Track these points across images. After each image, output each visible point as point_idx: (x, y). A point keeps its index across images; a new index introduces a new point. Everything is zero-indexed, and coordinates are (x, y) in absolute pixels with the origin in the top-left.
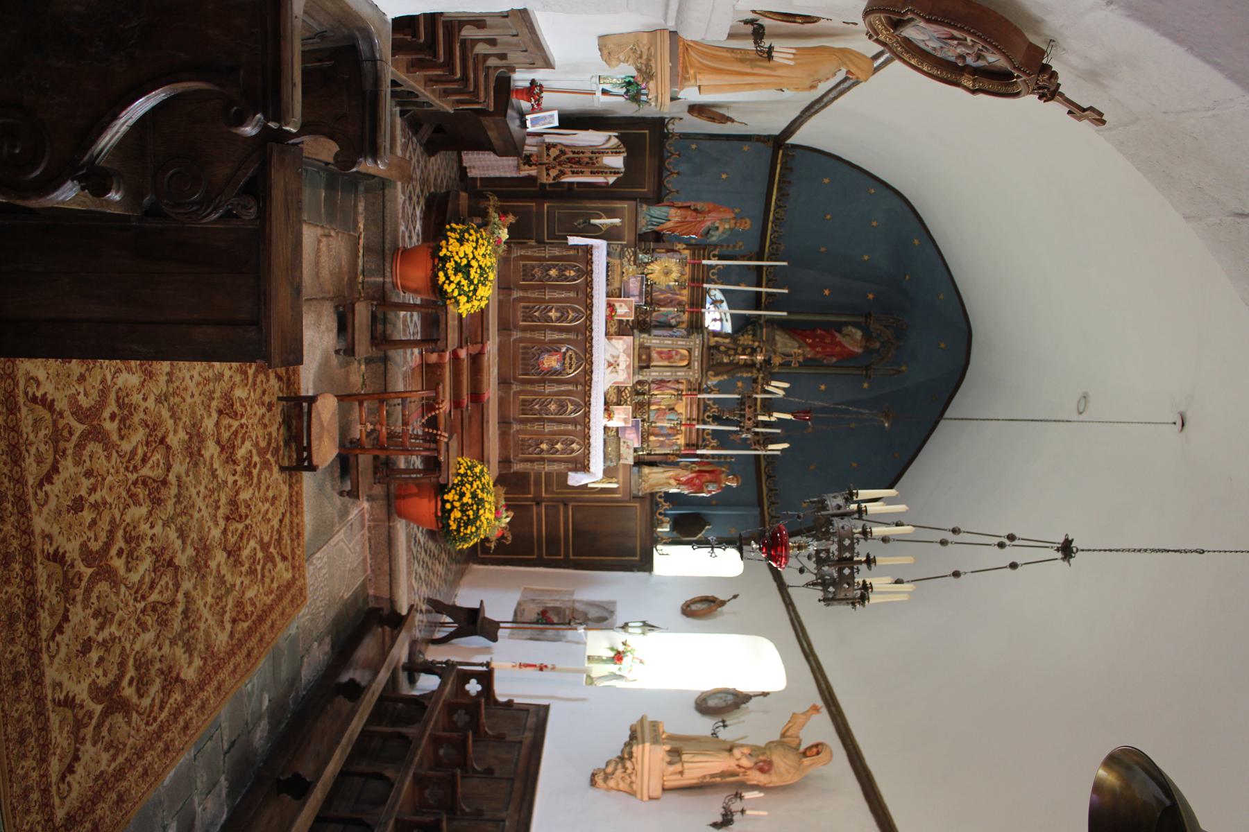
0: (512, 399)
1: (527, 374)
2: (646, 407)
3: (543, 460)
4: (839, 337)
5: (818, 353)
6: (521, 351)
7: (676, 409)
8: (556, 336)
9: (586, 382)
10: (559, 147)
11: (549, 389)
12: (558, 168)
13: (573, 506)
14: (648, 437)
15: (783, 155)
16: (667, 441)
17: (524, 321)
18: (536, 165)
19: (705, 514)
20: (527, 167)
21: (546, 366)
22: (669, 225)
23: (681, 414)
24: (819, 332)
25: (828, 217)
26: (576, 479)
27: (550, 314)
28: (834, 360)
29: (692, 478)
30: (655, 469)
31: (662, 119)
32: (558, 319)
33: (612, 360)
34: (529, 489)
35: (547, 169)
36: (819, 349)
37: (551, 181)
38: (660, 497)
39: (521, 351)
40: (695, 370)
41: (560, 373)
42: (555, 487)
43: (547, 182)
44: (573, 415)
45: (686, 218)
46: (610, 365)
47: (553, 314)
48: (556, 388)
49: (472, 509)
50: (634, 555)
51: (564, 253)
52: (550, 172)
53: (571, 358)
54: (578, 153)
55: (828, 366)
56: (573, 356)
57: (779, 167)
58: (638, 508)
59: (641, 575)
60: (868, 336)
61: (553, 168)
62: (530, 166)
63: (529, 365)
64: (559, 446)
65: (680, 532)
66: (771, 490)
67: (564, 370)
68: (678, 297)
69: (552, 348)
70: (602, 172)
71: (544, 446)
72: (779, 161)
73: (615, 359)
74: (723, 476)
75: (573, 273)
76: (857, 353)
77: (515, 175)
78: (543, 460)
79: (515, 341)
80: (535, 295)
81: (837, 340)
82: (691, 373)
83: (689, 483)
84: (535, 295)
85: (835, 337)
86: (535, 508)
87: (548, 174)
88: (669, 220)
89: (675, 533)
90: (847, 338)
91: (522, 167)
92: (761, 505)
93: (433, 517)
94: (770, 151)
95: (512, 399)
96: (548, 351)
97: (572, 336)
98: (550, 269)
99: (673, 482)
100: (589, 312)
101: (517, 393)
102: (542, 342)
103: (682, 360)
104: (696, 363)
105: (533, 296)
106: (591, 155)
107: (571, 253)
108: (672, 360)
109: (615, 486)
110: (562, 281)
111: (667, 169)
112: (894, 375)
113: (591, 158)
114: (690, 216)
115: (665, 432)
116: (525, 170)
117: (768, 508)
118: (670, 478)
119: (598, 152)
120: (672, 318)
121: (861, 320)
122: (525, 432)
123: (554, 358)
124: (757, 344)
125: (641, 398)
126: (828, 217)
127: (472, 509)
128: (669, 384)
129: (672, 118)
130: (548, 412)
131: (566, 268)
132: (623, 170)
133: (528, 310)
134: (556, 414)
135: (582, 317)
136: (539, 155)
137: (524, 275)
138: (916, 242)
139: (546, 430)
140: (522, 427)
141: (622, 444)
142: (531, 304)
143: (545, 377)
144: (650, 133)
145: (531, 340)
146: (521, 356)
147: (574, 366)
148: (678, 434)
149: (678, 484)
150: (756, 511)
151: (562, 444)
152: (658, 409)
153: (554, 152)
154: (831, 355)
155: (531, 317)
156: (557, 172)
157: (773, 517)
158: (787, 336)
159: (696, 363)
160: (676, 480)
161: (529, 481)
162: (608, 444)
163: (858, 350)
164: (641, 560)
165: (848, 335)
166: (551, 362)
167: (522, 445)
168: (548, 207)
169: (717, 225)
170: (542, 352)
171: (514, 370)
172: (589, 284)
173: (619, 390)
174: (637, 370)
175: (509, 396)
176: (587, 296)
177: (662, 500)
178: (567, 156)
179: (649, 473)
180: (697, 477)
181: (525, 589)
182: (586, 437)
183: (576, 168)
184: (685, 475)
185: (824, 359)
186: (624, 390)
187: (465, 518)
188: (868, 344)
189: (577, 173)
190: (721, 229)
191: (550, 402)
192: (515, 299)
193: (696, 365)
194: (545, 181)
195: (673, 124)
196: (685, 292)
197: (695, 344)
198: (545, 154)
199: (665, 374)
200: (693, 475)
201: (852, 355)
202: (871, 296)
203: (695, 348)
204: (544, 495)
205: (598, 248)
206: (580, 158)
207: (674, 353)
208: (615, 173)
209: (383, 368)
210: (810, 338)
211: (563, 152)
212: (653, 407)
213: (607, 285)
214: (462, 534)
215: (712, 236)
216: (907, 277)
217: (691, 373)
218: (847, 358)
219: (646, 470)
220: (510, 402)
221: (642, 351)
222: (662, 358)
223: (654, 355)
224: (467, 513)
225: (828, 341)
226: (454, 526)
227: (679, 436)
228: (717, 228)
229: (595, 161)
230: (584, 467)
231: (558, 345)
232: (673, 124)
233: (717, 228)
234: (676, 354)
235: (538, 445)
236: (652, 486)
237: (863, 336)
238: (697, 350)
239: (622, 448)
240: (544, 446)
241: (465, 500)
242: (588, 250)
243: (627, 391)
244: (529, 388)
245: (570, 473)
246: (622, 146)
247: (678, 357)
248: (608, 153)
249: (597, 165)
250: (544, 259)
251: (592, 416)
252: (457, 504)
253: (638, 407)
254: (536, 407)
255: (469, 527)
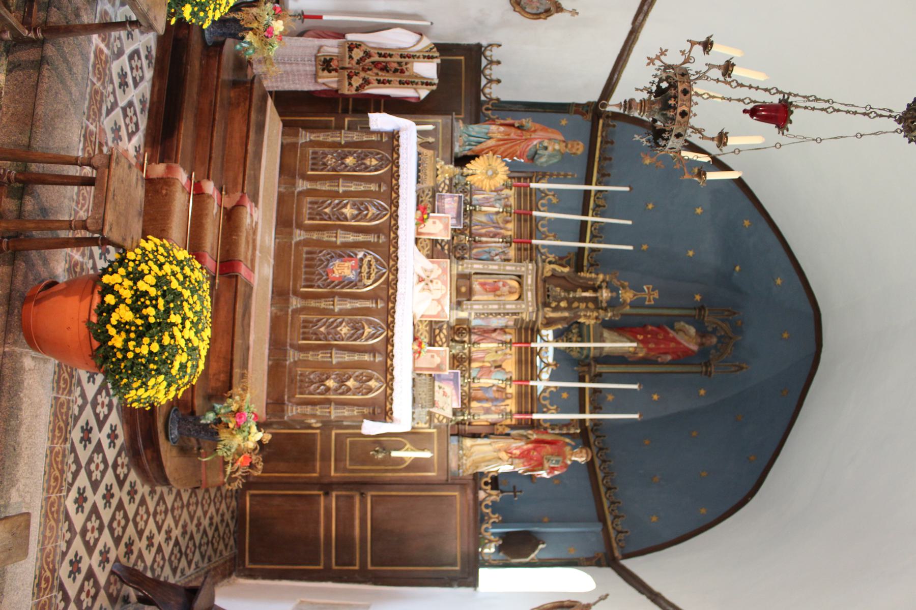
0: (290, 319)
1: (311, 287)
2: (466, 364)
3: (328, 402)
4: (672, 334)
5: (650, 350)
6: (304, 256)
7: (504, 366)
8: (351, 238)
9: (389, 297)
10: (363, 48)
11: (339, 305)
12: (362, 74)
13: (372, 496)
14: (469, 402)
15: (603, 124)
16: (493, 408)
17: (310, 219)
18: (336, 70)
19: (537, 533)
20: (326, 73)
21: (337, 275)
22: (491, 143)
23: (510, 372)
24: (650, 328)
25: (650, 206)
26: (371, 428)
27: (344, 210)
28: (669, 358)
29: (529, 451)
30: (479, 441)
31: (479, 46)
32: (354, 218)
33: (423, 275)
34: (314, 466)
35: (350, 77)
36: (652, 346)
37: (354, 92)
38: (487, 506)
39: (304, 256)
40: (528, 302)
41: (356, 285)
42: (348, 462)
43: (349, 93)
44: (371, 342)
45: (509, 135)
46: (421, 280)
47: (348, 211)
48: (349, 305)
49: (155, 307)
50: (454, 564)
51: (365, 139)
52: (353, 82)
53: (370, 266)
54: (385, 56)
55: (662, 364)
56: (373, 262)
57: (599, 140)
58: (458, 497)
59: (463, 592)
60: (702, 333)
61: (356, 74)
62: (330, 71)
63: (313, 273)
64: (351, 383)
65: (506, 553)
66: (613, 503)
67: (361, 281)
68: (502, 231)
69: (345, 252)
70: (412, 83)
71: (331, 383)
72: (599, 133)
73: (428, 273)
74: (568, 449)
75: (374, 162)
76: (693, 351)
77: (312, 87)
78: (328, 402)
79: (298, 244)
80: (326, 187)
81: (671, 335)
82: (523, 306)
83: (525, 455)
84: (326, 187)
85: (668, 333)
86: (322, 499)
87: (350, 84)
88: (490, 138)
89: (501, 554)
90: (681, 333)
91: (320, 73)
92: (602, 519)
93: (83, 327)
94: (588, 125)
95: (290, 319)
96: (340, 256)
97: (371, 238)
98: (346, 156)
99: (504, 455)
100: (394, 209)
101: (296, 311)
102: (333, 245)
103: (511, 293)
104: (529, 294)
105: (324, 188)
106: (400, 60)
107: (374, 138)
108: (498, 293)
109: (426, 454)
110: (360, 171)
111: (483, 113)
112: (736, 371)
113: (399, 63)
114: (514, 134)
115: (491, 394)
116: (323, 77)
117: (612, 523)
118: (499, 450)
119: (408, 56)
120: (496, 255)
121: (693, 312)
122: (305, 363)
123: (347, 264)
124: (601, 277)
125: (459, 347)
126: (650, 206)
127: (155, 307)
128: (494, 335)
129: (490, 45)
130: (337, 336)
131: (366, 156)
132: (436, 81)
133: (316, 206)
134: (348, 339)
135: (385, 215)
136: (341, 58)
137: (313, 164)
138: (747, 223)
139: (334, 361)
140: (302, 356)
141: (436, 388)
142: (321, 200)
143: (335, 290)
144: (465, 59)
145: (320, 243)
146: (304, 262)
147: (373, 276)
148: (507, 398)
149: (511, 457)
150: (598, 528)
151: (355, 380)
152: (482, 367)
153: (357, 54)
154: (666, 353)
155: (320, 215)
156: (361, 81)
157: (619, 532)
158: (616, 334)
159: (529, 294)
160: (507, 452)
161: (313, 454)
162: (418, 385)
163: (694, 347)
164: (463, 570)
165: (680, 330)
166: (343, 269)
167: (301, 381)
168: (348, 121)
169: (546, 144)
170: (332, 257)
171: (295, 281)
172: (394, 175)
173: (434, 327)
174: (455, 306)
175: (287, 314)
176: (392, 189)
177: (488, 511)
178: (372, 59)
179: (472, 446)
180: (534, 449)
181: (302, 602)
182: (387, 371)
183: (383, 76)
184: (518, 446)
185: (658, 357)
186: (439, 334)
187: (139, 322)
188: (704, 340)
189: (384, 82)
190: (550, 148)
191: (341, 323)
192: (300, 193)
193: (530, 296)
194: (346, 92)
195: (491, 51)
196: (510, 226)
197: (527, 269)
198: (347, 56)
199: (490, 307)
200: (530, 446)
201: (687, 352)
202: (698, 298)
203: (528, 274)
204: (333, 473)
205: (406, 129)
206: (387, 63)
207: (501, 284)
208: (427, 84)
209: (35, 77)
210: (641, 334)
211: (368, 54)
212: (474, 365)
213: (418, 182)
214: (130, 355)
215: (541, 156)
216: (738, 268)
217: (523, 306)
218: (683, 357)
219: (468, 442)
220: (286, 323)
221: (462, 281)
222: (486, 290)
223: (476, 287)
224: (145, 312)
225: (661, 337)
226: (118, 341)
227: (508, 402)
228: (546, 148)
229: (404, 68)
230: (383, 412)
231: (354, 250)
232: (491, 51)
233: (546, 148)
234: (504, 285)
235: (322, 382)
236: (476, 464)
237: (697, 332)
238: (530, 277)
239: (436, 394)
240: (331, 383)
241: (142, 286)
242: (394, 136)
243: (442, 335)
244: (313, 303)
245: (365, 421)
246: (435, 49)
247: (506, 289)
248: (419, 57)
249: (407, 73)
250: (339, 145)
251: (396, 339)
252: (127, 294)
253: (456, 364)
254: (322, 329)
255: (146, 340)
